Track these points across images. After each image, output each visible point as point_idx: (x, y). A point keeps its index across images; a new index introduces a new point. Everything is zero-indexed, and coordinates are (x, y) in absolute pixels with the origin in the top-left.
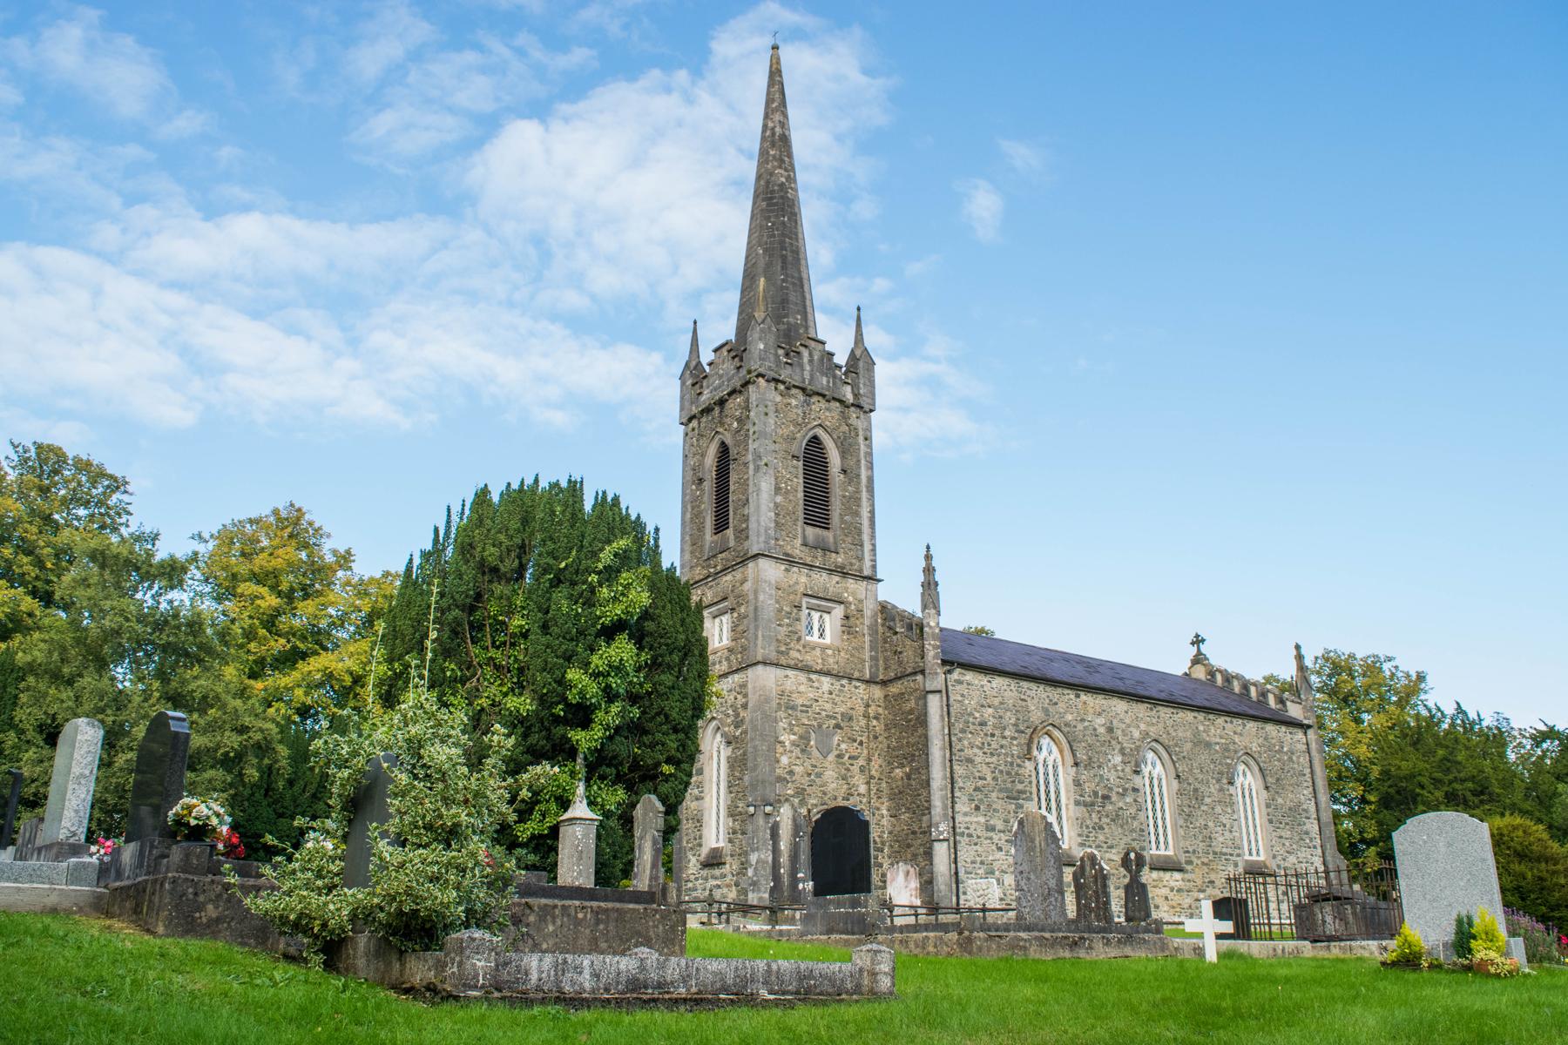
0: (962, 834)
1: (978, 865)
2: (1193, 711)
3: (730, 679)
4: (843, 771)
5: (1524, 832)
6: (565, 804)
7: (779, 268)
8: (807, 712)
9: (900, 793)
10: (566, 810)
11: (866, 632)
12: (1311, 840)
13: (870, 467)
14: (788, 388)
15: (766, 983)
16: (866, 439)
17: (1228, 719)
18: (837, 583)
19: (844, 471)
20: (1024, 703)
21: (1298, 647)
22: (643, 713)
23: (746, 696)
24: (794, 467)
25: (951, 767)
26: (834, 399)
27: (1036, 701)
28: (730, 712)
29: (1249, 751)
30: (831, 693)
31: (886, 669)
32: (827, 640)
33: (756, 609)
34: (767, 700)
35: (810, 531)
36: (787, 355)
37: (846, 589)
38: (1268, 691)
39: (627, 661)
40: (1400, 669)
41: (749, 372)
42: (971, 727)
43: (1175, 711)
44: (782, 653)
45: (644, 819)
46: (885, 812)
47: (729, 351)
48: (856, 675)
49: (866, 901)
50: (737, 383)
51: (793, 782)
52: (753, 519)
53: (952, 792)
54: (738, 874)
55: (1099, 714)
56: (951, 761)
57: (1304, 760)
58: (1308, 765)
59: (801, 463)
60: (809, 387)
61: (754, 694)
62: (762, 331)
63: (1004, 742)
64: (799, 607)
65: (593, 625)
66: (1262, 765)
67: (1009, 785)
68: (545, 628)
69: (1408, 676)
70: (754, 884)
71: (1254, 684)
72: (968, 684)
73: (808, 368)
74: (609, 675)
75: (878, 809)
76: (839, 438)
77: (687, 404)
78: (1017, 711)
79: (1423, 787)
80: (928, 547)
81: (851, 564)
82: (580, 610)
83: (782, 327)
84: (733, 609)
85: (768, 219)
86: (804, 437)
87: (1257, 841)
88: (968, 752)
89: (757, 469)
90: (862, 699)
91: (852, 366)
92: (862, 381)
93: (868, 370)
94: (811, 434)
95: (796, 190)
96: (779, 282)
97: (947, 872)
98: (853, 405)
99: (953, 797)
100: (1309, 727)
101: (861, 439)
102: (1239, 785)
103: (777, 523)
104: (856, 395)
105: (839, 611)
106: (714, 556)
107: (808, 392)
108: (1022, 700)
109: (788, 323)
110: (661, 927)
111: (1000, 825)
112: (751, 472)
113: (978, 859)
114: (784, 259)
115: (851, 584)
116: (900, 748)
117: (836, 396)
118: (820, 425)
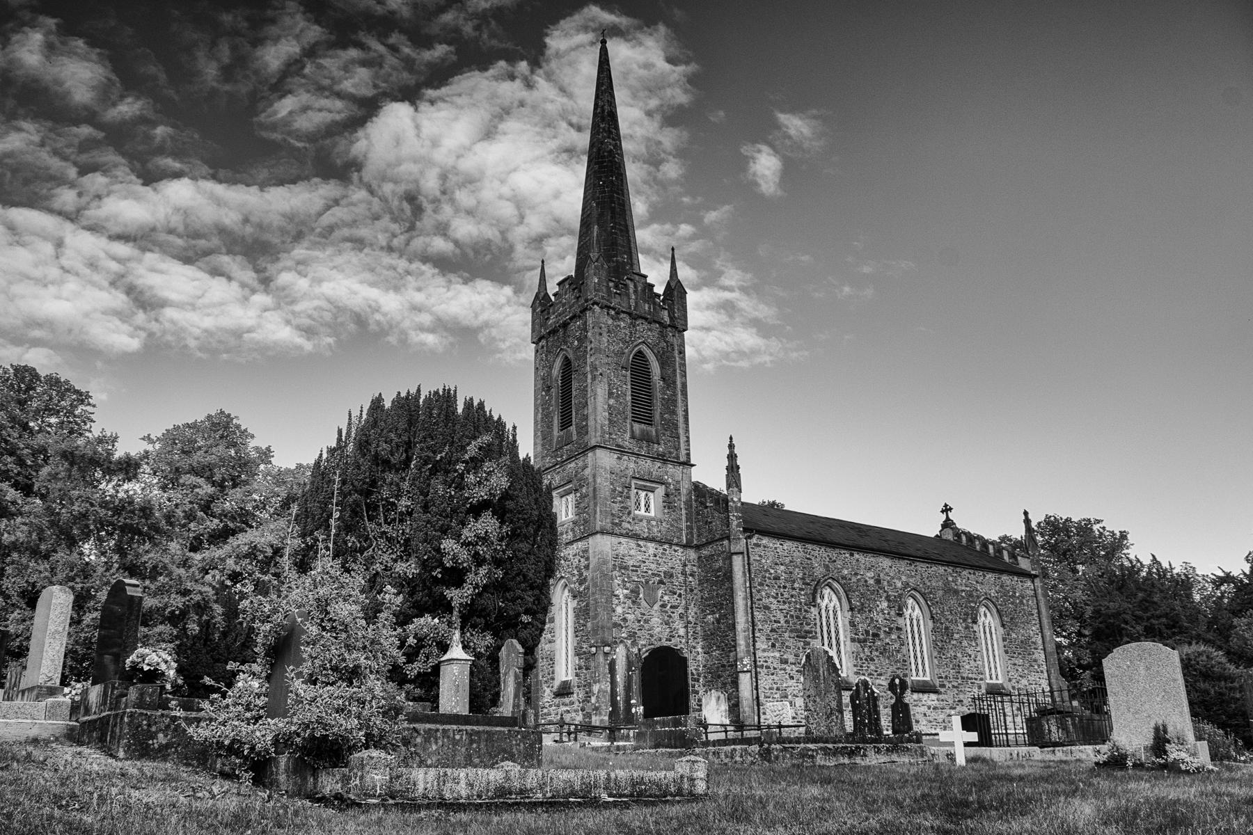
0: (762, 666)
1: (775, 691)
2: (943, 565)
3: (575, 546)
4: (666, 618)
5: (1208, 657)
6: (444, 648)
10: (445, 653)
12: (1039, 666)
13: (684, 375)
14: (617, 313)
15: (606, 788)
16: (680, 353)
17: (972, 571)
21: (1026, 513)
22: (505, 574)
23: (587, 559)
25: (752, 613)
28: (575, 572)
31: (699, 536)
32: (652, 514)
33: (595, 490)
34: (605, 562)
35: (637, 427)
37: (666, 473)
44: (616, 524)
45: (508, 659)
46: (700, 650)
47: (570, 285)
48: (676, 540)
49: (686, 721)
50: (577, 309)
52: (591, 418)
53: (753, 633)
55: (870, 569)
56: (752, 608)
64: (629, 488)
68: (426, 508)
70: (596, 709)
74: (477, 544)
80: (731, 438)
81: (670, 453)
84: (576, 490)
89: (594, 378)
99: (754, 637)
100: (1036, 576)
101: (676, 352)
104: (672, 318)
105: (661, 490)
106: (561, 448)
109: (617, 261)
112: (589, 381)
113: (775, 686)
114: (613, 211)
115: (670, 468)
116: (711, 598)
117: (656, 318)
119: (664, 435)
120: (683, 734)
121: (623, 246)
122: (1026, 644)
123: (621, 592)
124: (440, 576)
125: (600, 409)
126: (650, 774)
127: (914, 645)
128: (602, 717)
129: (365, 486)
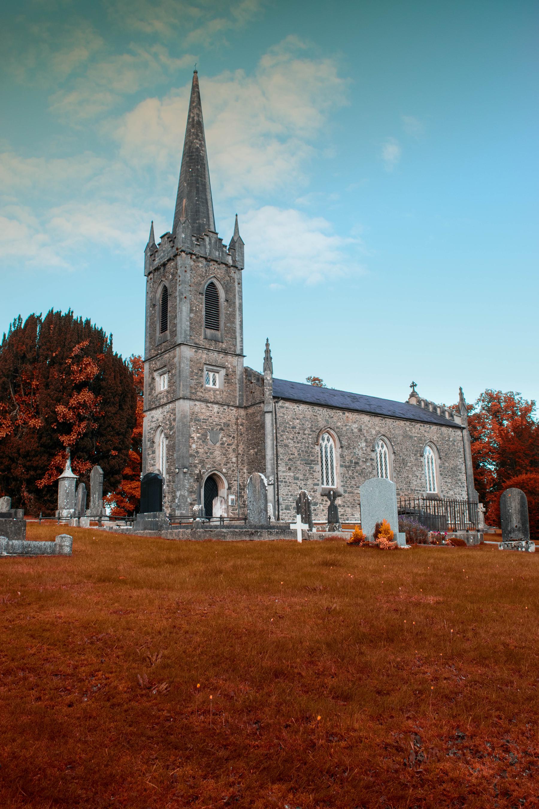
0: (282, 482)
1: (289, 496)
2: (404, 421)
3: (167, 406)
5: (535, 481)
6: (61, 471)
7: (195, 193)
8: (206, 422)
9: (253, 461)
10: (61, 473)
11: (237, 382)
12: (462, 483)
13: (241, 298)
14: (197, 258)
15: (6, 549)
16: (239, 284)
17: (422, 425)
18: (222, 358)
19: (227, 301)
20: (316, 418)
21: (461, 389)
22: (100, 426)
23: (175, 415)
24: (200, 299)
25: (277, 449)
26: (222, 263)
27: (321, 416)
28: (168, 423)
29: (432, 440)
30: (218, 413)
31: (247, 401)
32: (217, 387)
33: (180, 371)
34: (185, 417)
35: (209, 331)
36: (197, 240)
37: (227, 361)
38: (446, 411)
39: (88, 401)
40: (523, 398)
41: (177, 249)
42: (288, 429)
43: (394, 421)
44: (193, 393)
45: (94, 477)
46: (245, 471)
47: (168, 238)
48: (232, 404)
49: (159, 515)
50: (171, 255)
51: (198, 457)
52: (178, 326)
53: (277, 461)
54: (171, 502)
55: (355, 422)
56: (276, 446)
57: (460, 445)
58: (462, 447)
59: (204, 297)
60: (209, 257)
61: (179, 414)
62: (184, 227)
63: (305, 436)
64: (202, 370)
65: (71, 384)
66: (438, 447)
67: (307, 458)
68: (47, 386)
69: (527, 403)
70: (178, 506)
71: (439, 407)
72: (287, 408)
73: (208, 247)
74: (79, 408)
75: (242, 470)
76: (224, 283)
77: (148, 265)
78: (312, 421)
79: (520, 458)
80: (267, 340)
81: (230, 348)
82: (64, 377)
83: (196, 225)
84: (169, 371)
85: (190, 167)
86: (206, 283)
87: (434, 484)
88: (286, 442)
89: (181, 300)
90: (235, 416)
91: (232, 246)
92: (237, 254)
93: (241, 248)
94: (209, 282)
95: (205, 151)
96: (195, 201)
97: (273, 500)
98: (232, 266)
99: (277, 463)
100: (464, 428)
101: (236, 284)
102: (426, 457)
103: (191, 327)
104: (234, 261)
105: (223, 372)
106: (161, 344)
107: (208, 259)
108: (315, 416)
109: (199, 223)
110: (13, 528)
111: (301, 477)
112: (178, 302)
113: (290, 493)
114: (197, 189)
115: (229, 358)
116: (253, 439)
117: (223, 261)
118: (214, 277)
119: (226, 336)
120: (156, 523)
121: (204, 213)
122: (454, 470)
123: (195, 436)
124: (56, 428)
125: (184, 320)
126: (34, 543)
127: (381, 469)
128: (182, 511)
129: (10, 373)
